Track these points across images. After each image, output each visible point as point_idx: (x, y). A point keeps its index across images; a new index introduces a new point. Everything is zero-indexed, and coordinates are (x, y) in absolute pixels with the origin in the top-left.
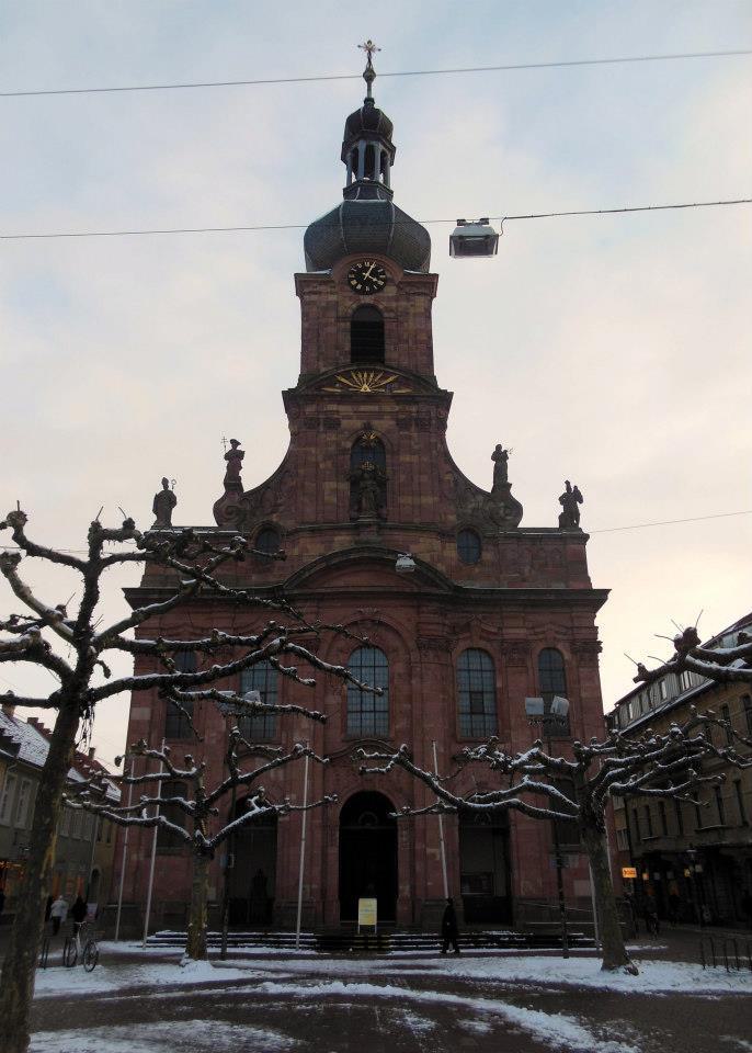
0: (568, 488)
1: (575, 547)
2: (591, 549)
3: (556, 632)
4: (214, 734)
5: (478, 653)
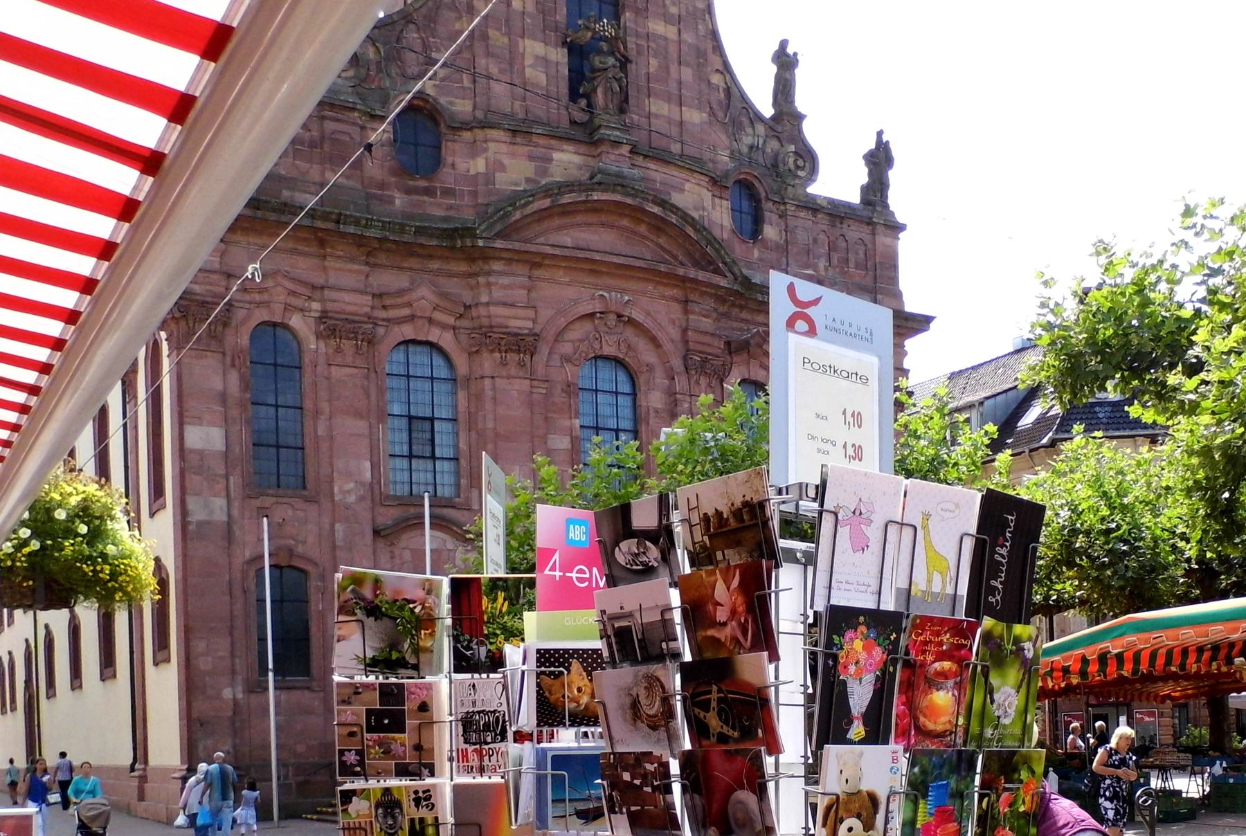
1: (888, 241)
2: (906, 246)
3: (292, 293)
4: (352, 485)
5: (426, 349)
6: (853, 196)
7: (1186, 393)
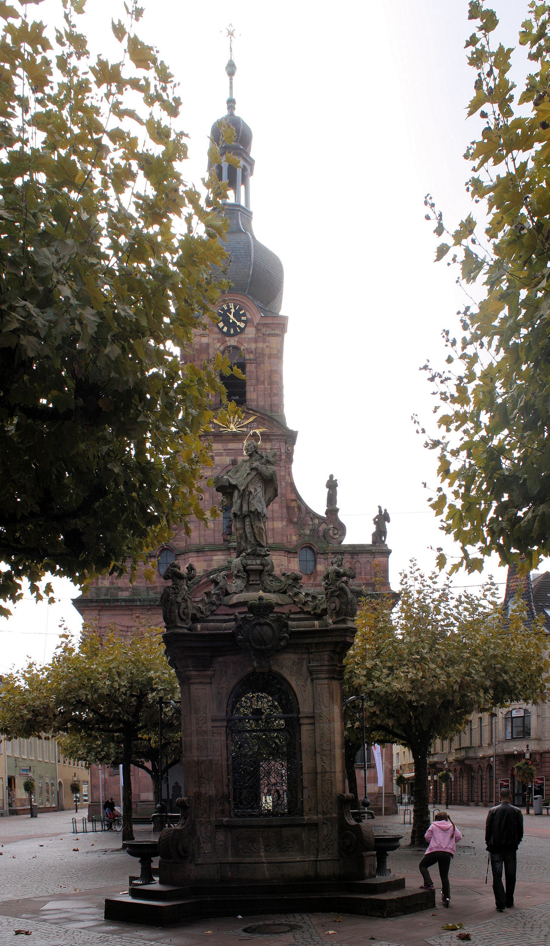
0: (380, 511)
3: (122, 631)
6: (368, 540)
7: (118, 199)
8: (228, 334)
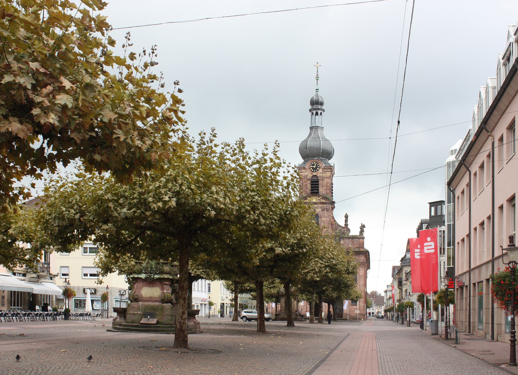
6: (358, 234)
8: (313, 171)
